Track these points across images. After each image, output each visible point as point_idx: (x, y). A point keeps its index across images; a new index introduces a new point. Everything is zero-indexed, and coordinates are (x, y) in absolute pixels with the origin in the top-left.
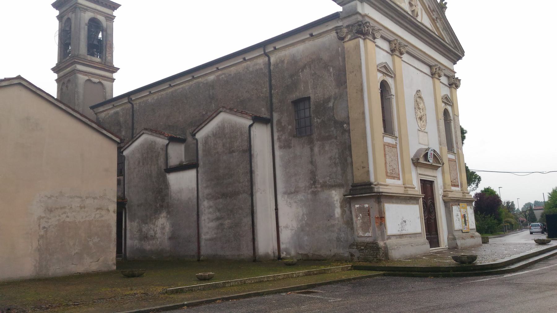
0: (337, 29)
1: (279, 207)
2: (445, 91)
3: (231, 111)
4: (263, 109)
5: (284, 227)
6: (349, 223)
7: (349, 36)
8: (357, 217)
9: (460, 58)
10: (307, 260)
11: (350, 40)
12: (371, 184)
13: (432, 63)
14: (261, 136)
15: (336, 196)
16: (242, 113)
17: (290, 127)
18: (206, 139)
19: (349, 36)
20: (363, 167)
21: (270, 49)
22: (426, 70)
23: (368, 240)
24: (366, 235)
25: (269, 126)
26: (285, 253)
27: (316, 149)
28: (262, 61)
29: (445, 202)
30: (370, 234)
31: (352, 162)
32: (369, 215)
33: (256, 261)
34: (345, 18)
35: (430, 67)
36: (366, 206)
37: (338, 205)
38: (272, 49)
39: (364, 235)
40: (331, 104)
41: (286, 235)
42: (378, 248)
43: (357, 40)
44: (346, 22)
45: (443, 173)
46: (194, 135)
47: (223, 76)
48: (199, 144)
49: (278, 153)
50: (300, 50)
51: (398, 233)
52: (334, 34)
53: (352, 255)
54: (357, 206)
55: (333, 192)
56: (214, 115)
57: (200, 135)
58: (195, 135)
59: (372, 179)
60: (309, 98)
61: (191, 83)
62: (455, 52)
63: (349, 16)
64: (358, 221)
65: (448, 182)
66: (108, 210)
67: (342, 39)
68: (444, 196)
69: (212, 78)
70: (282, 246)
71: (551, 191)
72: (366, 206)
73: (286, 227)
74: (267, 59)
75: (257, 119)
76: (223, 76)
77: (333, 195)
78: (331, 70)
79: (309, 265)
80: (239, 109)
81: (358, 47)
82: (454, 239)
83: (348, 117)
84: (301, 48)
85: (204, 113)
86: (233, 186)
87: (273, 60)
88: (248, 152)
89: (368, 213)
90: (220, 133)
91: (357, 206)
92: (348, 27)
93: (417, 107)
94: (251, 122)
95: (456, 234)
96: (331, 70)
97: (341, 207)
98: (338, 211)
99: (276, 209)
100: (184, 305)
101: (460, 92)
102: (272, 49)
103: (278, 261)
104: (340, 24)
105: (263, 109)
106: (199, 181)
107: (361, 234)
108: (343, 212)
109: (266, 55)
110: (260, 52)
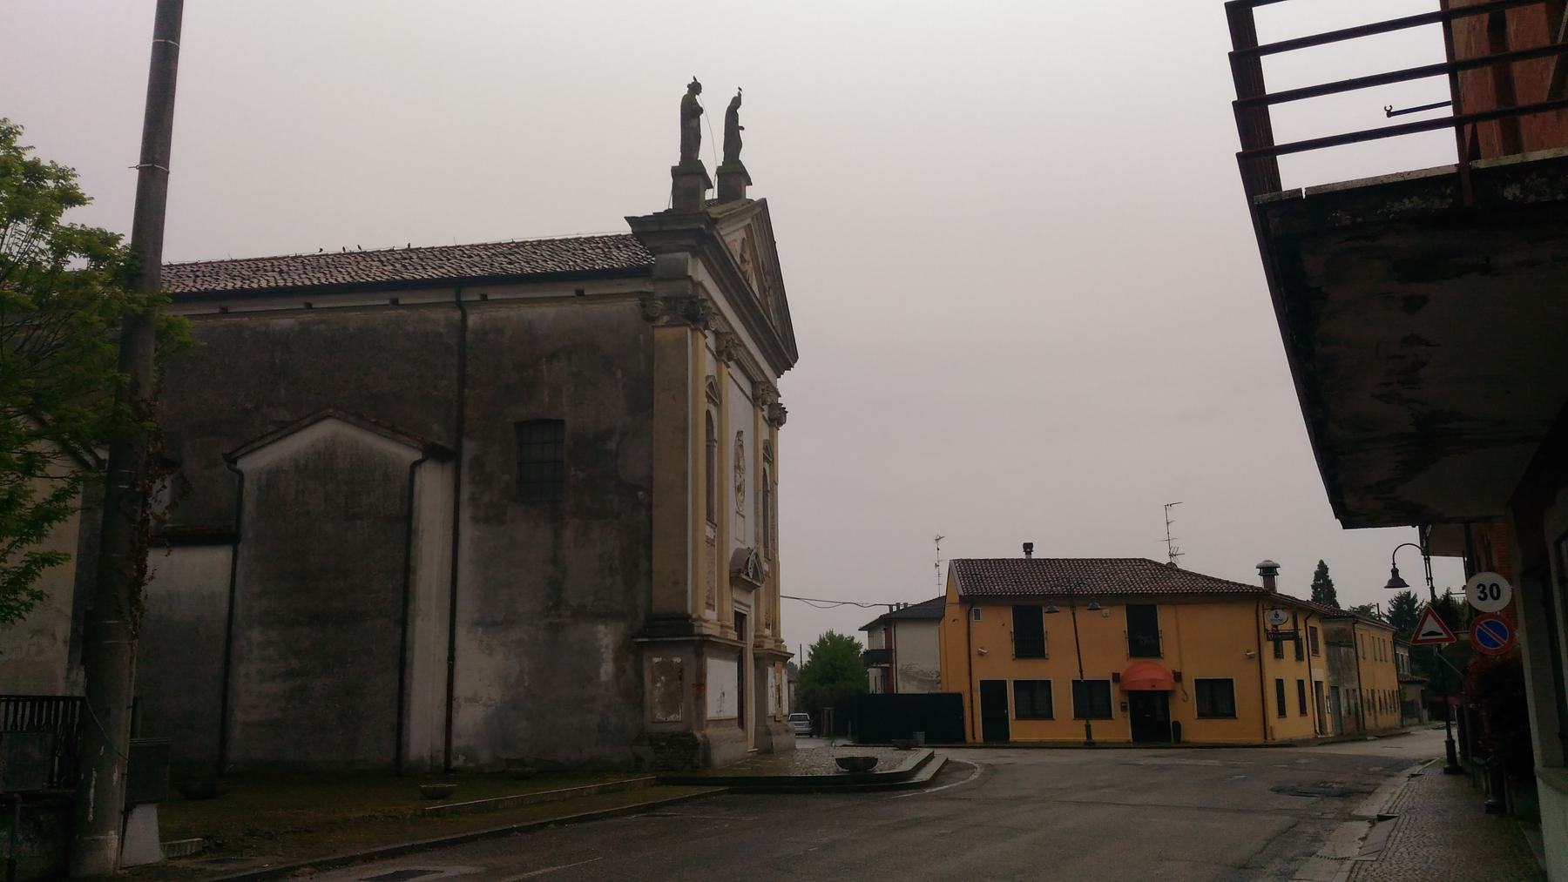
0: (645, 298)
1: (459, 654)
2: (764, 433)
3: (359, 419)
4: (436, 427)
5: (466, 700)
6: (634, 695)
7: (666, 319)
8: (654, 681)
9: (789, 367)
10: (510, 773)
11: (668, 325)
12: (689, 617)
13: (759, 378)
14: (433, 487)
15: (606, 637)
16: (395, 431)
17: (506, 477)
18: (272, 478)
19: (666, 319)
20: (675, 583)
21: (472, 296)
22: (748, 389)
23: (673, 728)
24: (672, 718)
25: (450, 466)
26: (462, 758)
27: (568, 534)
28: (441, 318)
29: (757, 659)
30: (679, 717)
31: (650, 573)
32: (681, 678)
33: (399, 771)
34: (661, 279)
35: (753, 383)
36: (677, 660)
37: (608, 655)
38: (477, 298)
39: (664, 718)
40: (612, 445)
41: (468, 718)
42: (696, 744)
43: (683, 329)
44: (662, 290)
45: (757, 599)
46: (232, 460)
47: (322, 326)
48: (247, 485)
49: (467, 532)
50: (547, 314)
51: (1393, 666)
52: (632, 305)
53: (639, 759)
54: (656, 660)
55: (601, 628)
56: (307, 421)
57: (254, 464)
58: (235, 461)
59: (690, 611)
60: (559, 423)
61: (211, 322)
62: (783, 353)
63: (670, 279)
64: (655, 690)
65: (763, 619)
66: (54, 637)
67: (650, 319)
68: (756, 646)
69: (286, 322)
70: (457, 743)
71: (815, 641)
72: (677, 660)
73: (473, 700)
74: (457, 315)
75: (436, 453)
76: (322, 326)
77: (600, 635)
78: (619, 374)
79: (516, 783)
80: (370, 411)
81: (681, 344)
82: (768, 733)
83: (650, 479)
84: (550, 311)
85: (249, 406)
86: (344, 595)
87: (473, 319)
88: (404, 522)
89: (680, 673)
90: (318, 467)
91: (656, 660)
92: (665, 299)
93: (737, 467)
94: (418, 456)
95: (770, 723)
96: (619, 374)
97: (616, 660)
98: (607, 669)
99: (451, 658)
100: (513, 830)
101: (783, 432)
102: (477, 298)
103: (446, 772)
104: (649, 288)
105: (436, 427)
106: (239, 579)
107: (659, 715)
108: (620, 671)
109: (461, 306)
110: (449, 296)
